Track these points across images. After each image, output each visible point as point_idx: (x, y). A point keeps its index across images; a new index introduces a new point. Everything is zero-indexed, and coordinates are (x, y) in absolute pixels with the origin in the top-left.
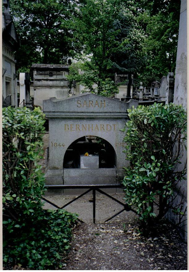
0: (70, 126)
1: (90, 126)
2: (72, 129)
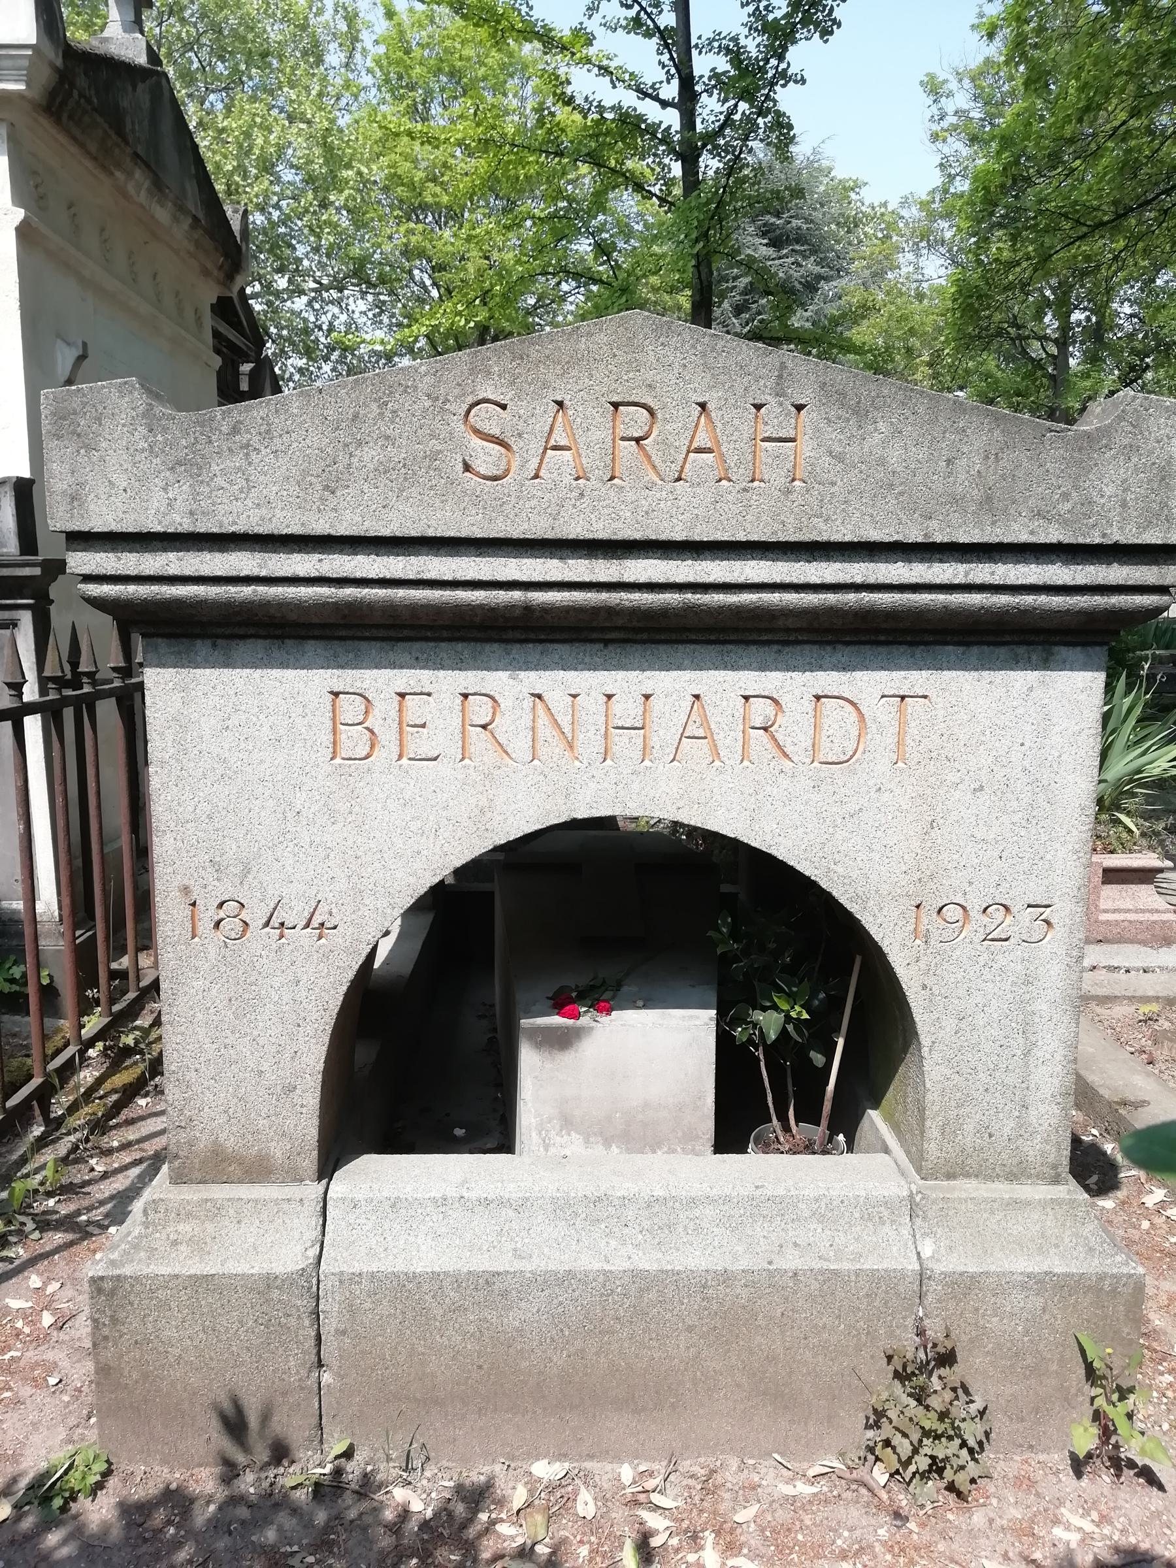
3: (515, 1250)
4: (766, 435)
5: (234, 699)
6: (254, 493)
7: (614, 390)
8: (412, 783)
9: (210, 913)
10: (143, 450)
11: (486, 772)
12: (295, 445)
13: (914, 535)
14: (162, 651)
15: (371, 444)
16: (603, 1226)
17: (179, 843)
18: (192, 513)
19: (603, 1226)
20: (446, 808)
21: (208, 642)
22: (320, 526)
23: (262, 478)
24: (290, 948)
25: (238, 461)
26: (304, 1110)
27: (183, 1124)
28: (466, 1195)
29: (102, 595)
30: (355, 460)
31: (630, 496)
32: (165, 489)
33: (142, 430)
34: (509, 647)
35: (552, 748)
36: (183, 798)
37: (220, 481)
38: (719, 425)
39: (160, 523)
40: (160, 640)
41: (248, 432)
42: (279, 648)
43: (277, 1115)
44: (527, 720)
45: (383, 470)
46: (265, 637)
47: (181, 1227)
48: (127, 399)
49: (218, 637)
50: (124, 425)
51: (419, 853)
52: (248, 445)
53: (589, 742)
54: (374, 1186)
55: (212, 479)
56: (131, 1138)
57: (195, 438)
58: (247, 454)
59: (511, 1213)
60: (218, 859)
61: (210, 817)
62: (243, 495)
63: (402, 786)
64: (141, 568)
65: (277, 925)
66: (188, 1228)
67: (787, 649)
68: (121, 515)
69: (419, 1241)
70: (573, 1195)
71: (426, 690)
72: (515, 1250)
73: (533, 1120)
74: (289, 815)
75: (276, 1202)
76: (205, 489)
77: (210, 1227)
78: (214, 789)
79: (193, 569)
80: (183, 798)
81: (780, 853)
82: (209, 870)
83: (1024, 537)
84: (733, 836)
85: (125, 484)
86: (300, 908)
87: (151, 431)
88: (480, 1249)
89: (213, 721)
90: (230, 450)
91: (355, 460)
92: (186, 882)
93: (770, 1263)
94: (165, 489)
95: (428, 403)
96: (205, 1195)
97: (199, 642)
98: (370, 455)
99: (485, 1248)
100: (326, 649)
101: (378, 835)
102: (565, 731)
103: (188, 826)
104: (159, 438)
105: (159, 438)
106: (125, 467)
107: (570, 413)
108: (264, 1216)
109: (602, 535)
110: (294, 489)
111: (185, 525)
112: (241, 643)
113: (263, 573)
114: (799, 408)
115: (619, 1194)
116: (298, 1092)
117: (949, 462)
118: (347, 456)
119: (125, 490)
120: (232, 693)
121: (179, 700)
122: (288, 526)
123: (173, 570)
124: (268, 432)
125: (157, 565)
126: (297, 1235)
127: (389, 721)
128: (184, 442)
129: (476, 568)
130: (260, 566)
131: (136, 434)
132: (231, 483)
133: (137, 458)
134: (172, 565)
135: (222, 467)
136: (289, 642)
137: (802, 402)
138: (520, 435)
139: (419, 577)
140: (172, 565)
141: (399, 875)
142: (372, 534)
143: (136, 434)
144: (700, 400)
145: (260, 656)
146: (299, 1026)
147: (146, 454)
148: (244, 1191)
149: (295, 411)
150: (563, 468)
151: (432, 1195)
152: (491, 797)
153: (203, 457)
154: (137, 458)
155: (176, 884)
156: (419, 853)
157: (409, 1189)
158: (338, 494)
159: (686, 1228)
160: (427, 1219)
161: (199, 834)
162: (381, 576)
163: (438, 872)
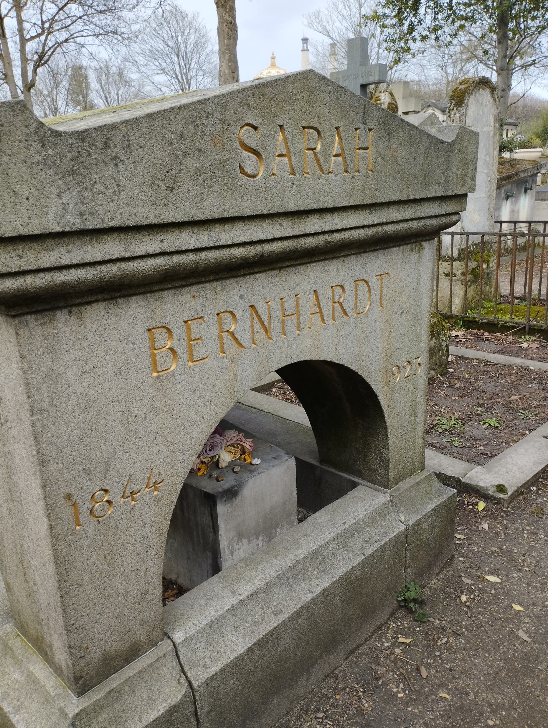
0: (179, 331)
1: (290, 305)
2: (199, 352)
3: (273, 612)
4: (360, 146)
5: (88, 350)
6: (123, 195)
7: (304, 120)
8: (197, 376)
9: (86, 505)
10: (38, 163)
11: (232, 358)
12: (146, 157)
13: (405, 197)
14: (32, 325)
15: (191, 155)
16: (300, 577)
17: (61, 466)
18: (81, 214)
19: (300, 577)
20: (214, 386)
21: (66, 311)
22: (167, 217)
23: (128, 183)
24: (138, 505)
25: (110, 171)
26: (154, 602)
27: (82, 655)
28: (241, 598)
29: (5, 289)
30: (183, 167)
31: (312, 183)
32: (59, 196)
33: (36, 146)
34: (238, 280)
35: (261, 336)
36: (60, 432)
37: (99, 187)
38: (344, 141)
39: (59, 224)
40: (29, 317)
41: (115, 147)
42: (114, 305)
43: (139, 614)
44: (248, 323)
45: (198, 173)
46: (104, 300)
47: (100, 719)
48: (20, 118)
49: (72, 306)
50: (20, 141)
51: (203, 417)
52: (116, 158)
53: (275, 326)
54: (195, 622)
55: (93, 186)
56: (131, 674)
57: (79, 152)
58: (116, 165)
59: (263, 595)
60: (88, 466)
61: (80, 439)
62: (116, 197)
63: (192, 379)
64: (40, 263)
65: (129, 494)
66: (105, 716)
67: (346, 259)
68: (27, 221)
69: (230, 636)
70: (285, 569)
71: (200, 316)
72: (273, 612)
73: (225, 543)
74: (131, 419)
75: (151, 665)
76: (88, 194)
77: (117, 706)
78: (81, 418)
79: (79, 258)
80: (60, 432)
81: (345, 363)
82: (83, 476)
83: (434, 194)
84: (329, 360)
85: (27, 194)
86: (142, 478)
87: (43, 146)
88: (258, 622)
89: (75, 369)
90: (104, 161)
91: (183, 167)
92: (68, 491)
93: (364, 554)
94: (59, 196)
95: (220, 126)
96: (107, 689)
97: (58, 313)
98: (192, 163)
99: (260, 620)
100: (143, 301)
101: (182, 414)
102: (265, 324)
103: (65, 450)
104: (50, 152)
105: (50, 152)
106: (25, 179)
107: (286, 133)
108: (146, 678)
109: (301, 208)
110: (149, 191)
111: (78, 224)
112: (89, 307)
113: (128, 255)
114: (370, 130)
115: (301, 558)
116: (150, 592)
117: (414, 158)
118: (178, 165)
119: (27, 199)
120: (85, 345)
121: (49, 360)
122: (147, 219)
123: (65, 261)
124: (128, 146)
125: (52, 258)
126: (169, 676)
127: (182, 341)
128: (70, 155)
129: (243, 234)
130: (125, 250)
131: (32, 149)
132: (107, 188)
133: (35, 171)
134: (64, 258)
135: (100, 175)
136: (120, 301)
137: (371, 127)
138: (265, 148)
139: (216, 244)
140: (64, 258)
141: (194, 435)
142: (196, 219)
143: (32, 149)
144: (337, 126)
145: (102, 314)
146: (147, 551)
147: (41, 166)
148: (130, 671)
149: (145, 130)
150: (285, 168)
151: (226, 608)
152: (235, 372)
153: (85, 167)
154: (35, 171)
155: (61, 495)
156: (203, 417)
157: (213, 614)
158: (175, 192)
159: (328, 558)
160: (228, 622)
161: (73, 453)
162: (196, 247)
163: (213, 425)
